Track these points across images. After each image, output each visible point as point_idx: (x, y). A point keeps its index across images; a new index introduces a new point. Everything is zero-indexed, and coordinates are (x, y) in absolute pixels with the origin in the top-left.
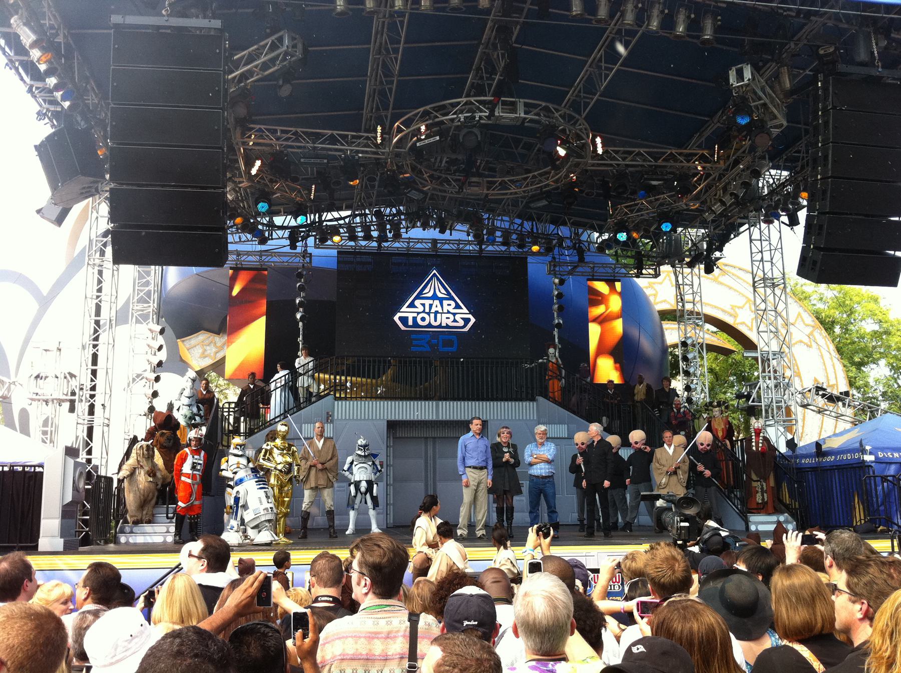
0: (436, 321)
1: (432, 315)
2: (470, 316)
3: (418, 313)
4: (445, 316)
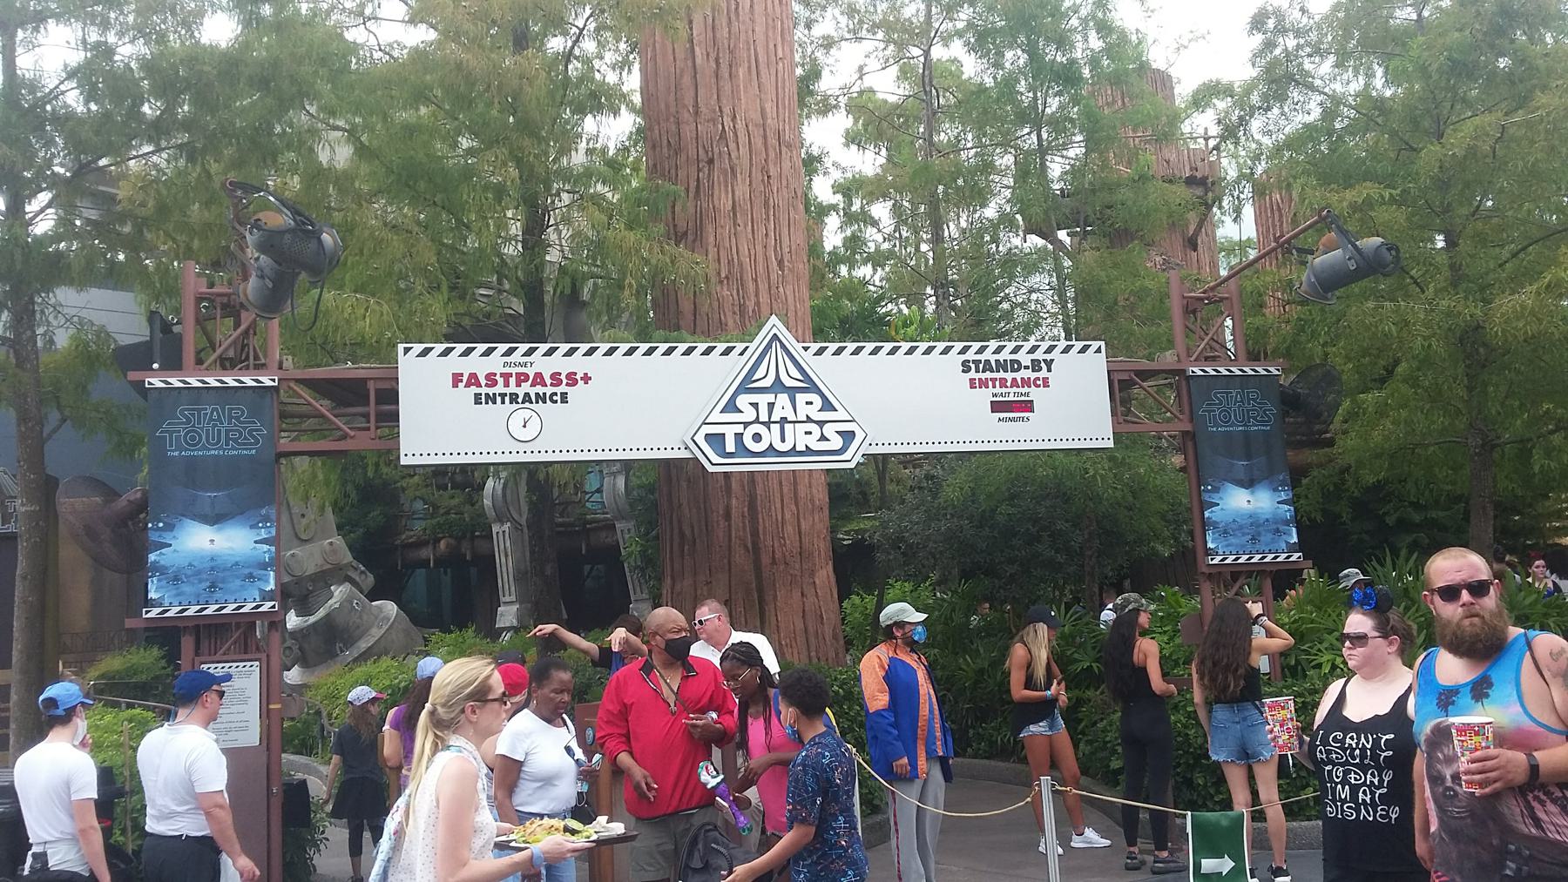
0: (783, 440)
3: (746, 425)
4: (802, 428)
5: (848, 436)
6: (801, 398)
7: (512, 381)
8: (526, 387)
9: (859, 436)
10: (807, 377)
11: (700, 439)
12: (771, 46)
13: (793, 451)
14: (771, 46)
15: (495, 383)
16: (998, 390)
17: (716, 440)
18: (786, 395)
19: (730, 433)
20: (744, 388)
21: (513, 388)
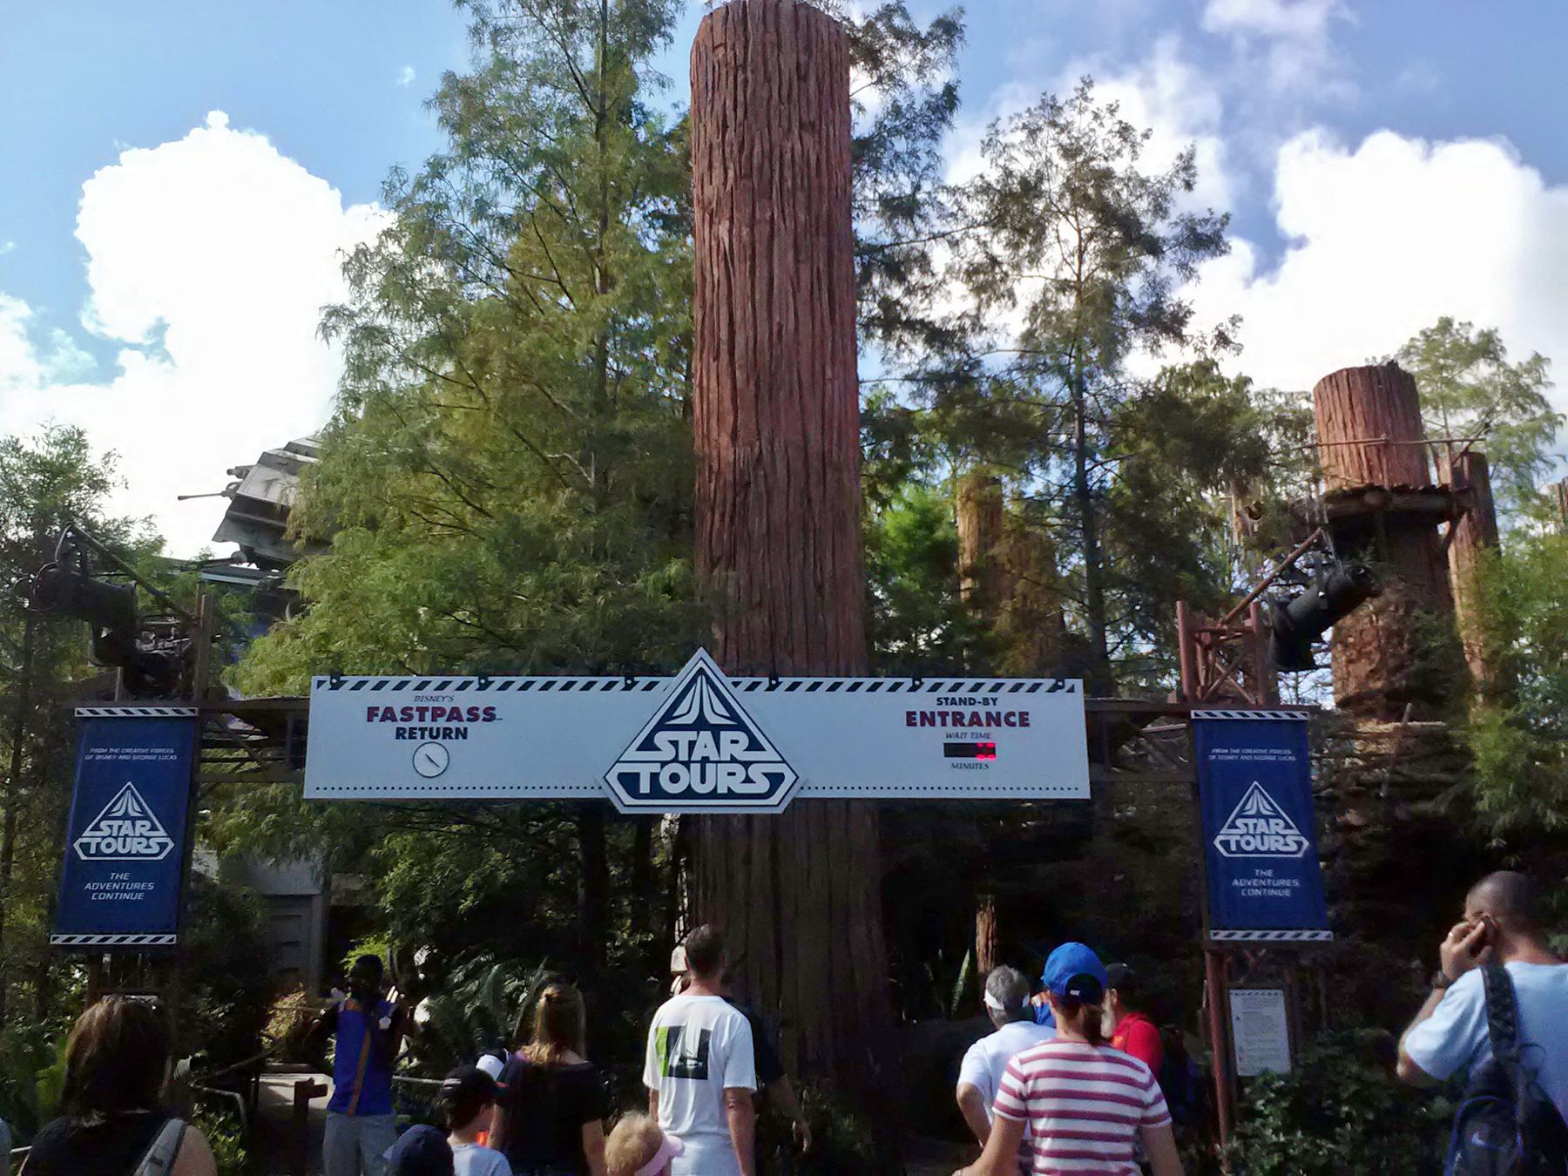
0: (703, 781)
1: (696, 768)
2: (1303, 839)
3: (664, 764)
4: (724, 769)
5: (775, 780)
6: (726, 736)
7: (428, 715)
8: (442, 723)
9: (789, 778)
10: (733, 715)
11: (613, 778)
12: (818, 367)
13: (713, 794)
14: (818, 367)
15: (410, 718)
16: (950, 728)
17: (630, 781)
18: (709, 733)
19: (645, 772)
20: (662, 726)
21: (428, 723)
